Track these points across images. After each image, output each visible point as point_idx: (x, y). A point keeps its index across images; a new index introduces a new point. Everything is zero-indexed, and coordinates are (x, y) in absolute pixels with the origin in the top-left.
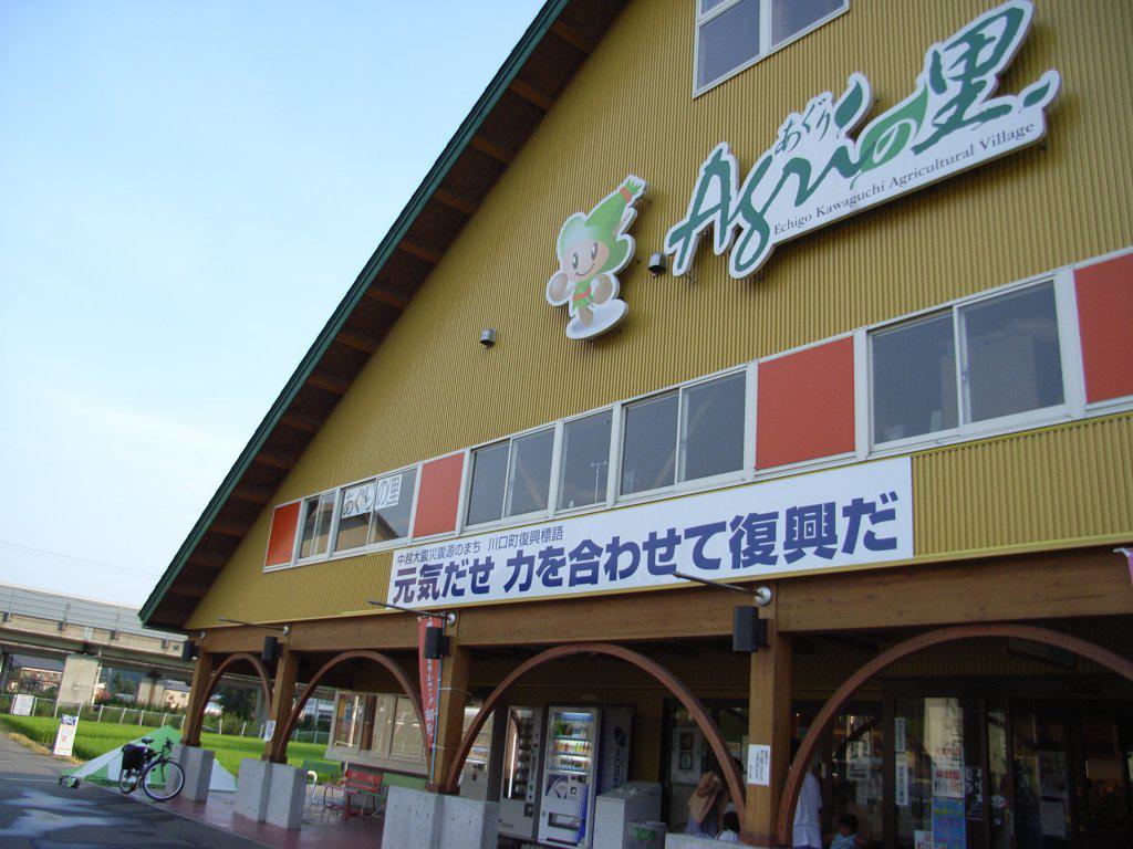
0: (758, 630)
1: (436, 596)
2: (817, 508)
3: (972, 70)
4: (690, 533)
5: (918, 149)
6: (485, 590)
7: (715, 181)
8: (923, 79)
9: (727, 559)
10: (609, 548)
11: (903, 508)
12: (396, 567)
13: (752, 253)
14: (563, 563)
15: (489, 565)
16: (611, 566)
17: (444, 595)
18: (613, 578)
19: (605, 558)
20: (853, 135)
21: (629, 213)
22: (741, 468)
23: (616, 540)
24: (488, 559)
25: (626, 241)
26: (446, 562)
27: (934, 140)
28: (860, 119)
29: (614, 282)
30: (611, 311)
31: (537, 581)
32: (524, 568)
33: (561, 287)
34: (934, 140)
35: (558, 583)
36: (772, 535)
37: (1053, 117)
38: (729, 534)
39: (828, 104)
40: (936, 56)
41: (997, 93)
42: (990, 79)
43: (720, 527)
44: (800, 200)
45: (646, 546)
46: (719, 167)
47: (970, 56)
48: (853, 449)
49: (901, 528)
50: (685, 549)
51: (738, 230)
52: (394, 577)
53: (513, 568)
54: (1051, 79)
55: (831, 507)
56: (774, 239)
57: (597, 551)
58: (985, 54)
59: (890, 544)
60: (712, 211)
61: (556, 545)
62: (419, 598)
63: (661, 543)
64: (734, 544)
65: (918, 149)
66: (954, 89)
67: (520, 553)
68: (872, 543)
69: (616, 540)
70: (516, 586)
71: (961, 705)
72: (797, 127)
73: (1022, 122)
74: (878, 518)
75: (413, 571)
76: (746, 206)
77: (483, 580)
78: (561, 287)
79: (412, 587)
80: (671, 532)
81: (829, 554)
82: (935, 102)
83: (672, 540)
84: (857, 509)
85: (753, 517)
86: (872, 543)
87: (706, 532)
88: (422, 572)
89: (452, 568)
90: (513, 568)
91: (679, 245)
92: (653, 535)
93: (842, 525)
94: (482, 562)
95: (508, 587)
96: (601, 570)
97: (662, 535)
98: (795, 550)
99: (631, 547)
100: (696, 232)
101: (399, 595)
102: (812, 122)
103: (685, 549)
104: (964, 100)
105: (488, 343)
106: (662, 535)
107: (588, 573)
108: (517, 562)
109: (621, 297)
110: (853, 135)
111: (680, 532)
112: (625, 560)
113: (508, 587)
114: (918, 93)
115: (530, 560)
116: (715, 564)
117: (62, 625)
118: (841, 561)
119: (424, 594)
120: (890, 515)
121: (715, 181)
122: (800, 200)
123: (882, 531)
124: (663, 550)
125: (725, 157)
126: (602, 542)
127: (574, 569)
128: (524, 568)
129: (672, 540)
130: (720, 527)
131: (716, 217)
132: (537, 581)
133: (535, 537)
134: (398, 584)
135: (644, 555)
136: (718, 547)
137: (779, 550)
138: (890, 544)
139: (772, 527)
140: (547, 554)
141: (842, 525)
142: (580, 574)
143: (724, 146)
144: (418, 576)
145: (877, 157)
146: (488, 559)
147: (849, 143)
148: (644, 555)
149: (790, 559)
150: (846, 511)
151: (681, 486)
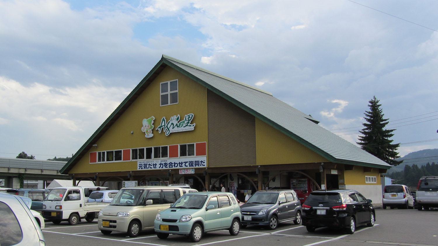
0: (206, 173)
1: (147, 168)
2: (198, 161)
3: (189, 120)
4: (184, 162)
5: (184, 127)
6: (156, 168)
7: (163, 122)
8: (185, 119)
9: (188, 166)
10: (174, 163)
11: (206, 162)
12: (138, 164)
13: (167, 133)
14: (168, 165)
15: (156, 164)
16: (174, 166)
17: (149, 168)
18: (175, 167)
19: (173, 164)
20: (178, 122)
21: (153, 122)
22: (150, 158)
23: (175, 162)
24: (156, 164)
25: (152, 126)
26: (148, 164)
27: (185, 126)
28: (179, 120)
29: (151, 131)
30: (151, 135)
31: (164, 167)
32: (162, 165)
33: (144, 129)
34: (185, 126)
35: (167, 167)
36: (193, 164)
37: (195, 128)
38: (188, 163)
39: (176, 117)
40: (186, 117)
41: (190, 124)
42: (190, 121)
43: (188, 162)
44: (173, 128)
45: (179, 163)
46: (163, 120)
47: (189, 118)
48: (178, 157)
49: (205, 164)
50: (184, 164)
51: (166, 130)
52: (138, 165)
53: (160, 165)
54: (194, 124)
55: (199, 161)
56: (170, 132)
57: (173, 164)
58: (190, 119)
59: (204, 165)
60: (163, 126)
61: (166, 162)
62: (144, 168)
63: (181, 163)
64: (189, 164)
65: (184, 127)
66: (187, 121)
67: (161, 163)
68: (151, 168)
69: (175, 162)
70: (161, 167)
71: (25, 180)
72: (172, 119)
73: (192, 128)
74: (203, 163)
75: (142, 164)
76: (167, 126)
77: (156, 166)
78: (144, 129)
79: (142, 167)
80: (182, 162)
81: (199, 166)
82: (186, 122)
83: (182, 163)
84: (201, 162)
85: (191, 161)
86: (151, 168)
87: (186, 162)
88: (144, 165)
89: (149, 165)
90: (160, 165)
91: (159, 129)
92: (180, 162)
93: (200, 163)
94: (155, 164)
95: (159, 168)
96: (173, 166)
97: (155, 164)
98: (196, 165)
99: (177, 163)
100: (161, 128)
101: (140, 168)
102: (174, 119)
103: (184, 164)
104: (188, 123)
105: (132, 134)
106: (181, 162)
107: (170, 166)
108: (161, 164)
109: (152, 133)
110: (178, 122)
111: (183, 162)
112: (176, 165)
113: (159, 168)
114: (184, 120)
115: (163, 164)
116: (187, 166)
117: (42, 170)
118: (200, 167)
119: (145, 168)
120: (204, 162)
121: (163, 122)
122: (173, 128)
123: (151, 167)
124: (155, 166)
125: (164, 119)
126: (173, 162)
127: (169, 166)
128: (162, 165)
129: (182, 163)
130: (188, 162)
131: (164, 127)
132: (164, 167)
133: (163, 161)
134: (140, 166)
135: (179, 165)
136: (187, 164)
137: (194, 165)
138: (204, 165)
139: (193, 163)
140: (165, 164)
141: (200, 163)
142: (170, 166)
143: (165, 117)
144: (143, 165)
145: (180, 126)
146: (156, 164)
147: (178, 123)
148: (179, 165)
149: (195, 166)
150: (200, 162)
151: (187, 156)
